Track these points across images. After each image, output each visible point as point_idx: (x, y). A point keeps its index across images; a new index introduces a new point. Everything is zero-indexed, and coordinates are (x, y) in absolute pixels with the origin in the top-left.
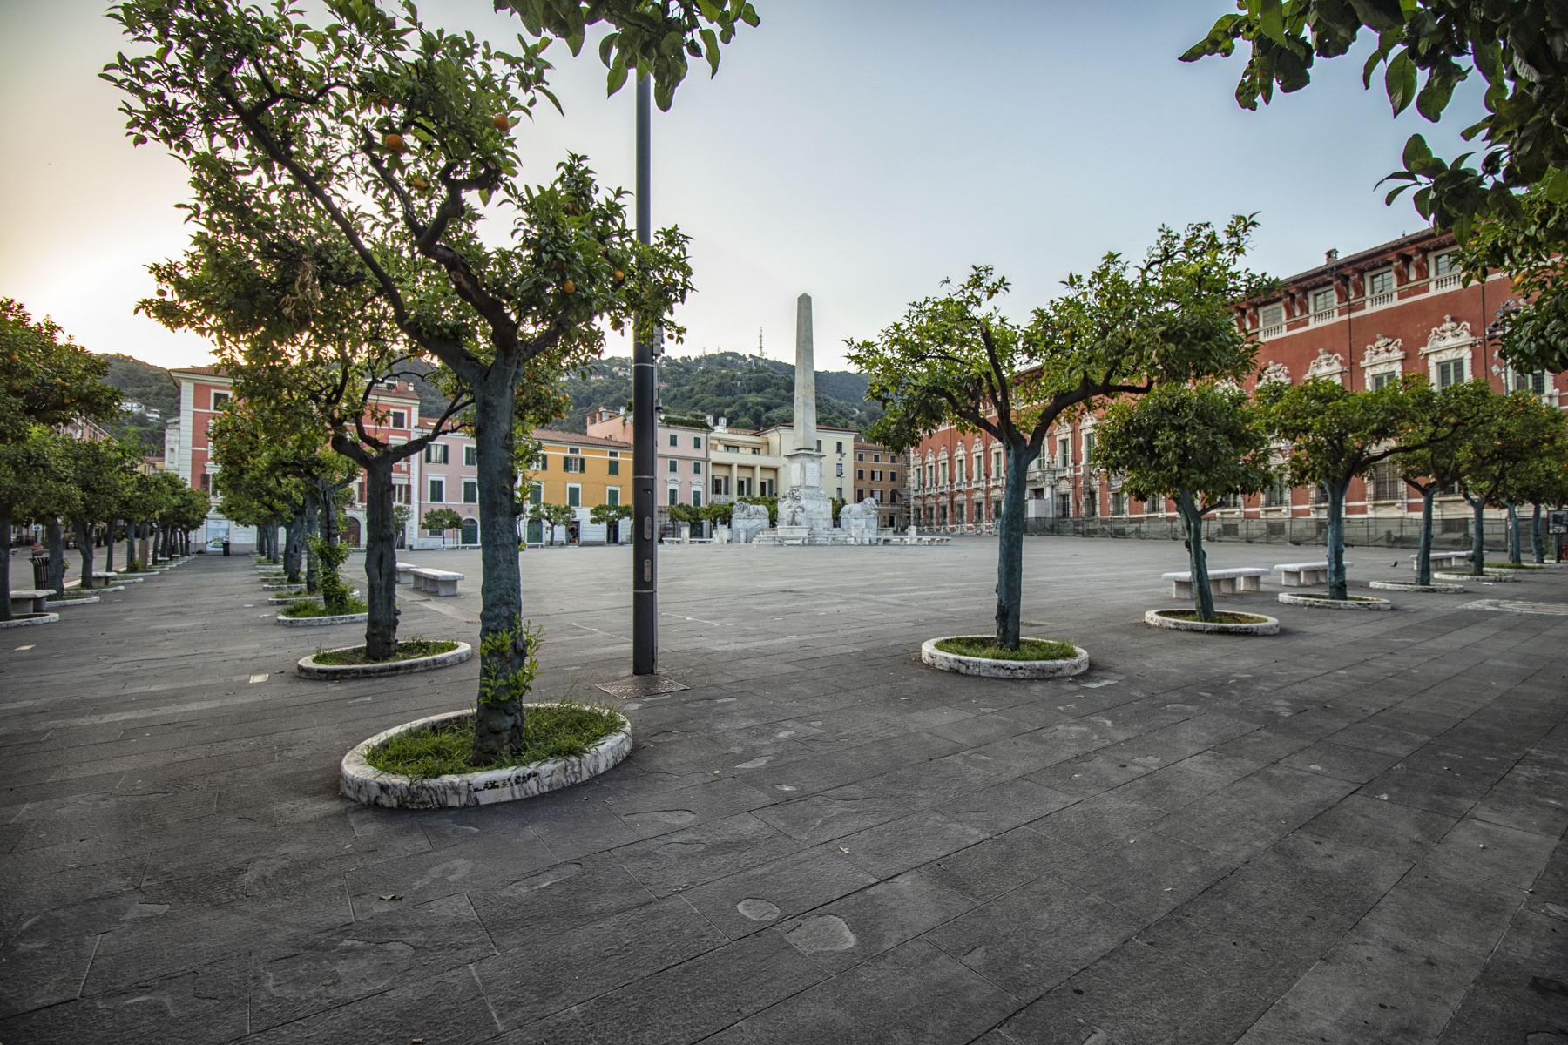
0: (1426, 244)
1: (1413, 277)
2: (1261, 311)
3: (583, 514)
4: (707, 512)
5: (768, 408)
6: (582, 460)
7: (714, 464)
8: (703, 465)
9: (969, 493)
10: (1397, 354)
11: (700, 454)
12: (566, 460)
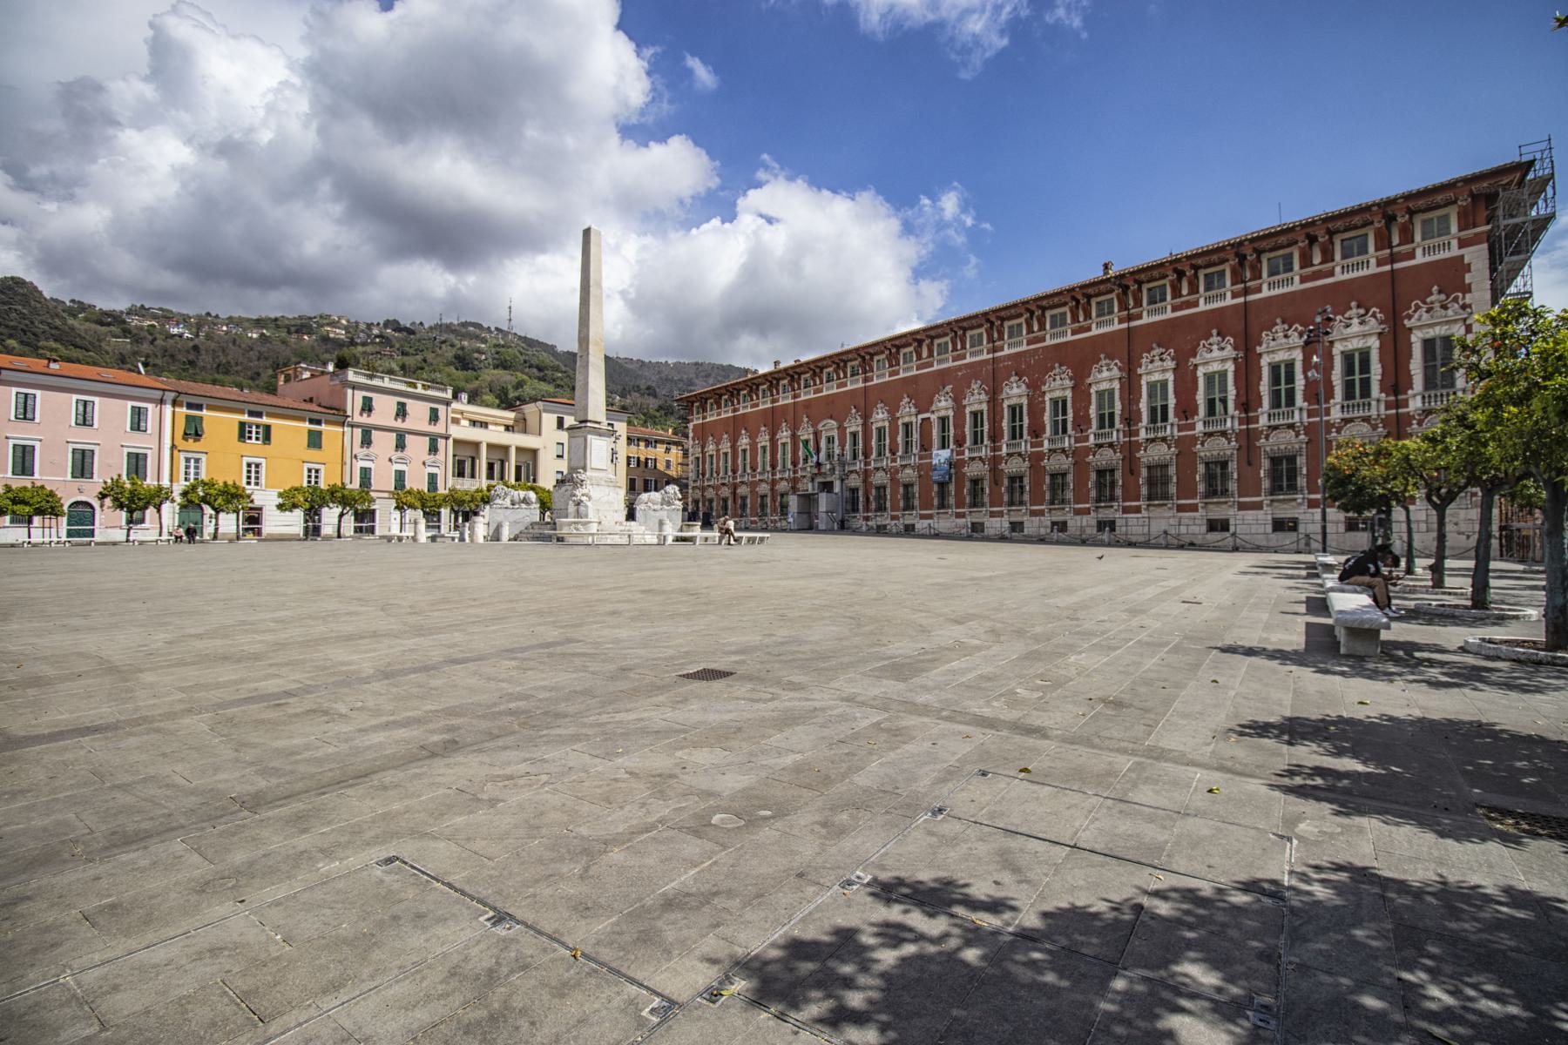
1: (1317, 259)
2: (1418, 221)
3: (265, 498)
4: (445, 499)
6: (268, 428)
7: (456, 442)
8: (441, 442)
9: (753, 485)
11: (439, 428)
12: (242, 425)
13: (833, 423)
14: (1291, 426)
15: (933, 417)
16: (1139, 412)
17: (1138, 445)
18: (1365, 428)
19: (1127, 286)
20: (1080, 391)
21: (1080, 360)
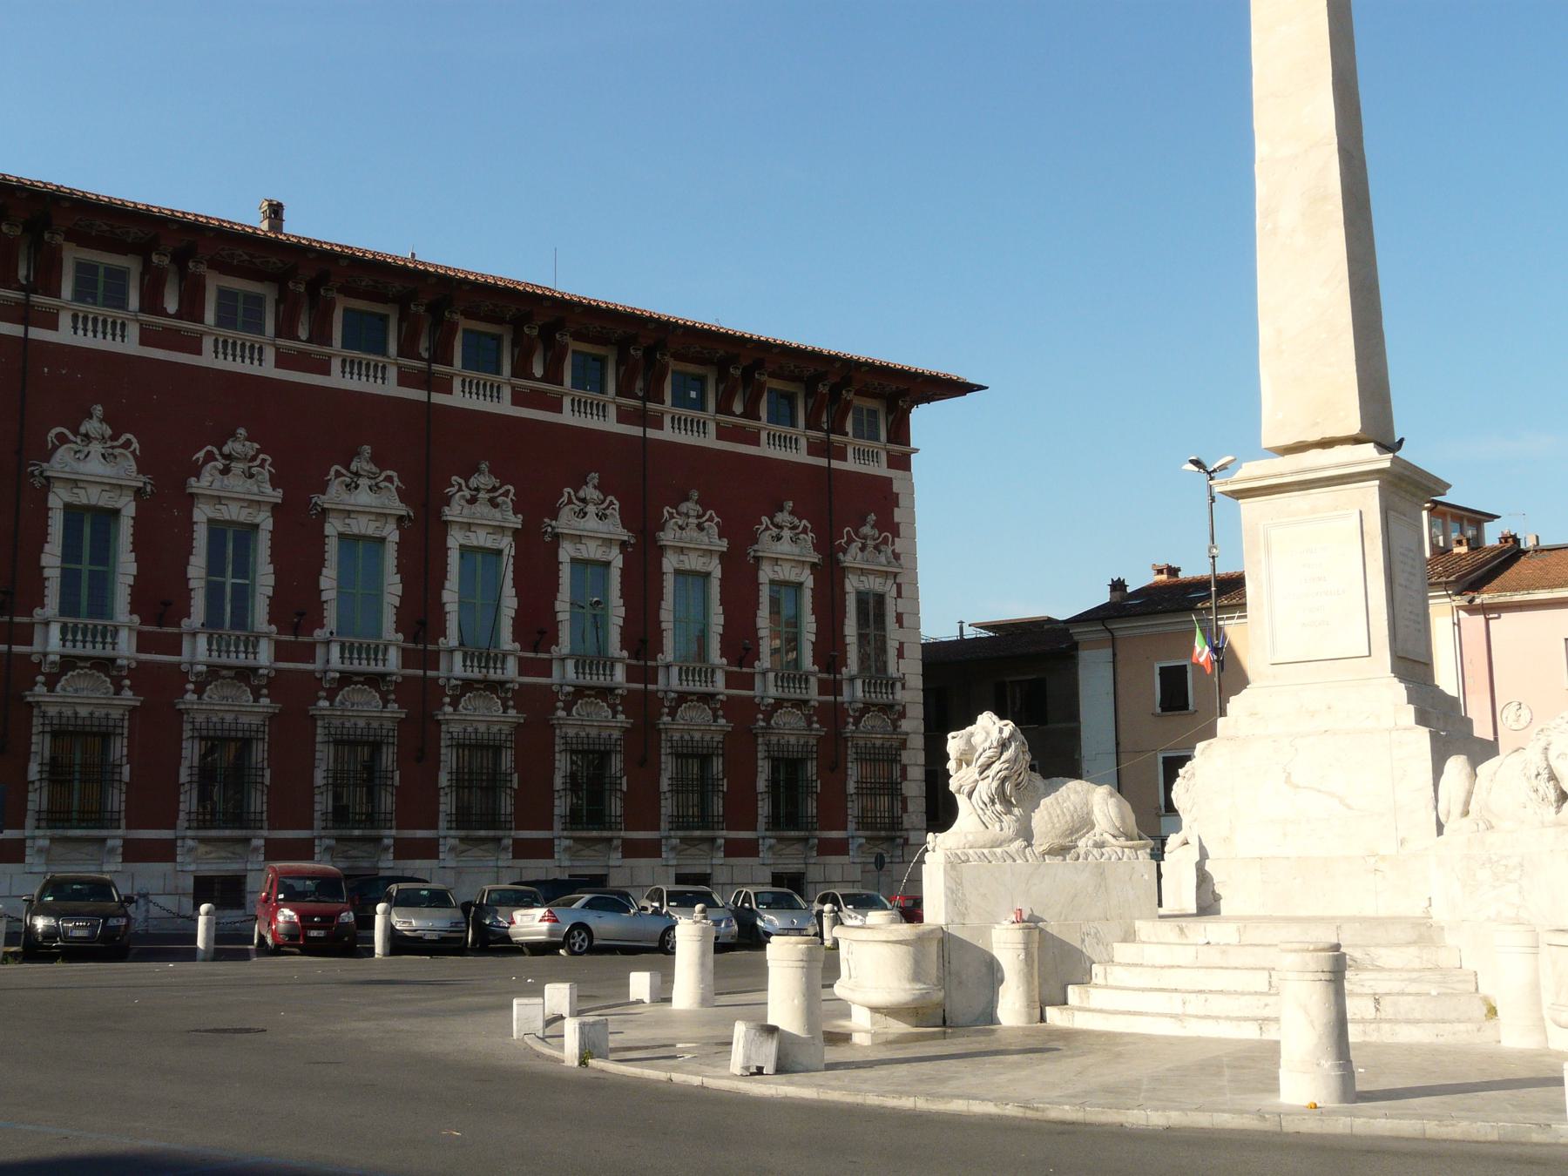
1: (738, 407)
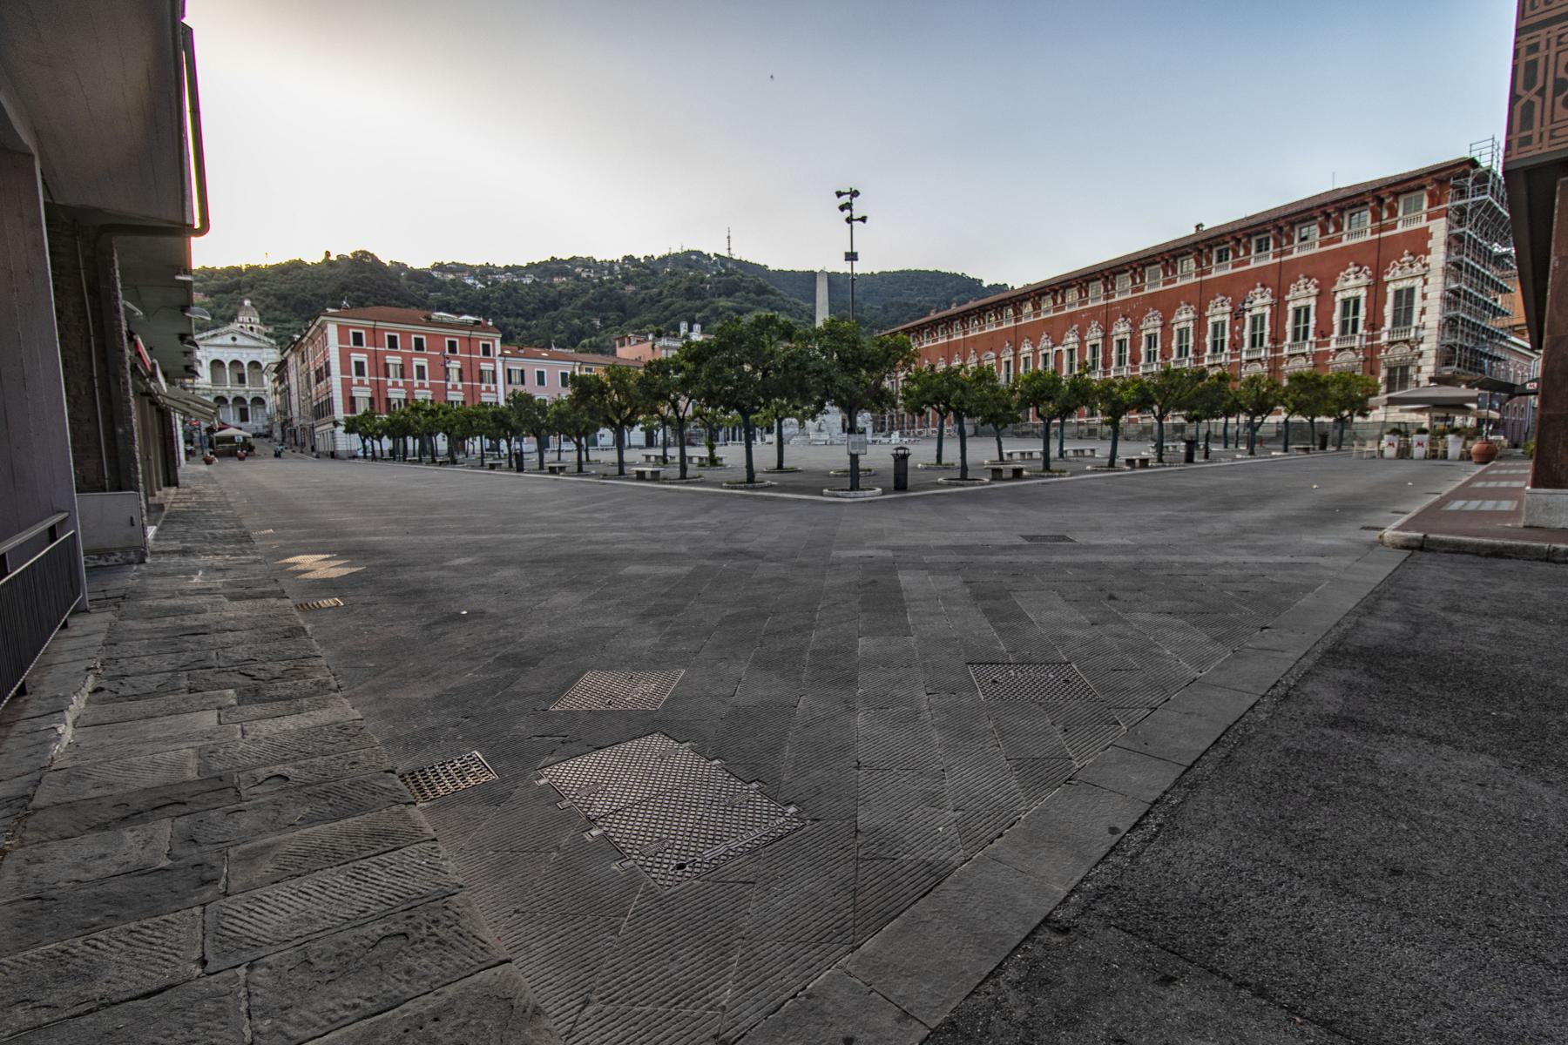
0: (1399, 188)
1: (1331, 230)
5: (740, 312)
10: (1228, 308)
13: (993, 354)
14: (1303, 354)
15: (1064, 349)
16: (1205, 345)
17: (1281, 360)
18: (1351, 355)
19: (1206, 245)
20: (1166, 327)
21: (1166, 305)
